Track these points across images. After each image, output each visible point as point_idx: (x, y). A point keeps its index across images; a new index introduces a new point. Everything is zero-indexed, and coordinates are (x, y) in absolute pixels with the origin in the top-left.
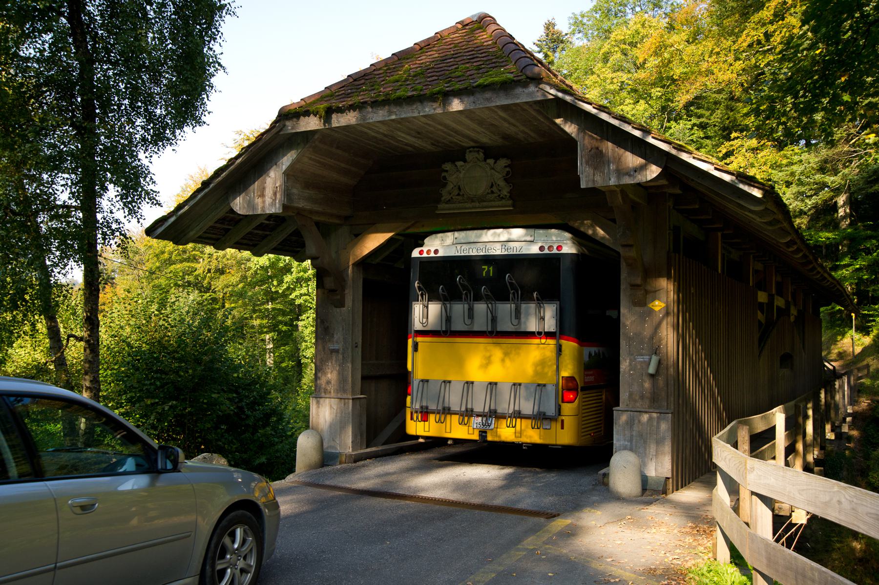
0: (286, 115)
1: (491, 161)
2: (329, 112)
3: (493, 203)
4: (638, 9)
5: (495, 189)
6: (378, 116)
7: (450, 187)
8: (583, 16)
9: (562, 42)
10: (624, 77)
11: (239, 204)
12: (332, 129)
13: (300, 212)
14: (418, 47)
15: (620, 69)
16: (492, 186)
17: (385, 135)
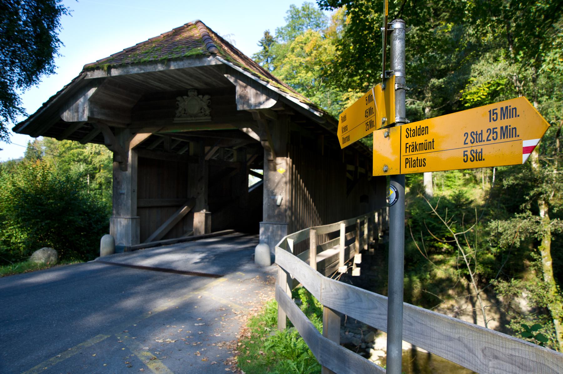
0: (87, 69)
1: (201, 96)
2: (110, 68)
3: (201, 118)
4: (309, 27)
5: (202, 111)
6: (135, 70)
7: (180, 109)
8: (282, 29)
9: (273, 41)
10: (302, 60)
11: (67, 116)
12: (111, 77)
13: (99, 121)
14: (162, 36)
15: (299, 55)
16: (201, 109)
17: (143, 81)
